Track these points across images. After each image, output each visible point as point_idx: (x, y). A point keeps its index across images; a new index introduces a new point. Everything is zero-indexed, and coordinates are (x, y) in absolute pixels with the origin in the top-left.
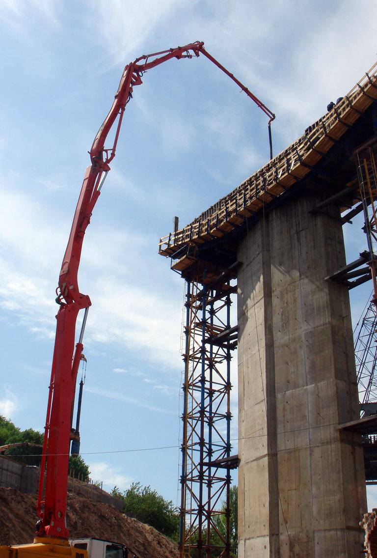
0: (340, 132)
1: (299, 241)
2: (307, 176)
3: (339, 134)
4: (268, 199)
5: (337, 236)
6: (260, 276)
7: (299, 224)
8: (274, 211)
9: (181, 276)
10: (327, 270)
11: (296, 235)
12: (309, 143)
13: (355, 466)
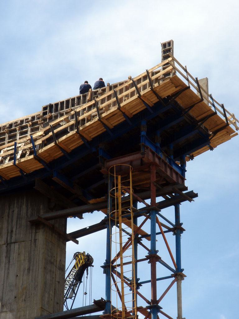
0: (96, 132)
1: (8, 257)
2: (36, 172)
5: (58, 260)
7: (12, 231)
10: (42, 308)
12: (51, 134)
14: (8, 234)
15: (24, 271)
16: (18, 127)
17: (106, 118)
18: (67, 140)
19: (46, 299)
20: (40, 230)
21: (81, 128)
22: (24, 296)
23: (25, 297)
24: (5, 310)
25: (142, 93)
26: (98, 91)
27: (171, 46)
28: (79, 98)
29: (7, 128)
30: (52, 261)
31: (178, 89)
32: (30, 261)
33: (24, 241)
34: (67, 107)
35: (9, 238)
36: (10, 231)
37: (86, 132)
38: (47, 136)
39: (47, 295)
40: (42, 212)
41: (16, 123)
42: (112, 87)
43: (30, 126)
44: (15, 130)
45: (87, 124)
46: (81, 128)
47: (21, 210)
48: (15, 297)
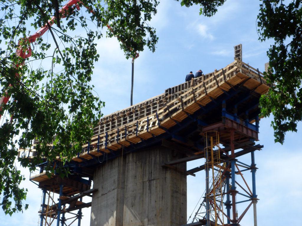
0: (195, 109)
1: (150, 189)
2: (162, 135)
3: (194, 110)
4: (127, 144)
5: (182, 189)
6: (114, 212)
7: (152, 172)
8: (131, 155)
9: (38, 186)
10: (171, 222)
11: (148, 182)
12: (167, 111)
13: (243, 142)
14: (149, 174)
15: (160, 198)
16: (151, 104)
17: (199, 100)
18: (177, 115)
19: (174, 216)
20: (168, 172)
21: (185, 108)
22: (160, 214)
23: (161, 215)
24: (150, 223)
25: (220, 84)
26: (197, 79)
27: (240, 48)
28: (186, 84)
29: (145, 104)
30: (177, 190)
31: (243, 80)
32: (163, 192)
33: (159, 179)
34: (180, 90)
35: (150, 177)
36: (150, 172)
37: (188, 110)
38: (166, 113)
39: (174, 213)
40: (169, 161)
41: (150, 101)
42: (206, 76)
43: (159, 103)
44: (149, 106)
45: (188, 105)
46: (185, 108)
47: (156, 159)
48: (156, 215)
